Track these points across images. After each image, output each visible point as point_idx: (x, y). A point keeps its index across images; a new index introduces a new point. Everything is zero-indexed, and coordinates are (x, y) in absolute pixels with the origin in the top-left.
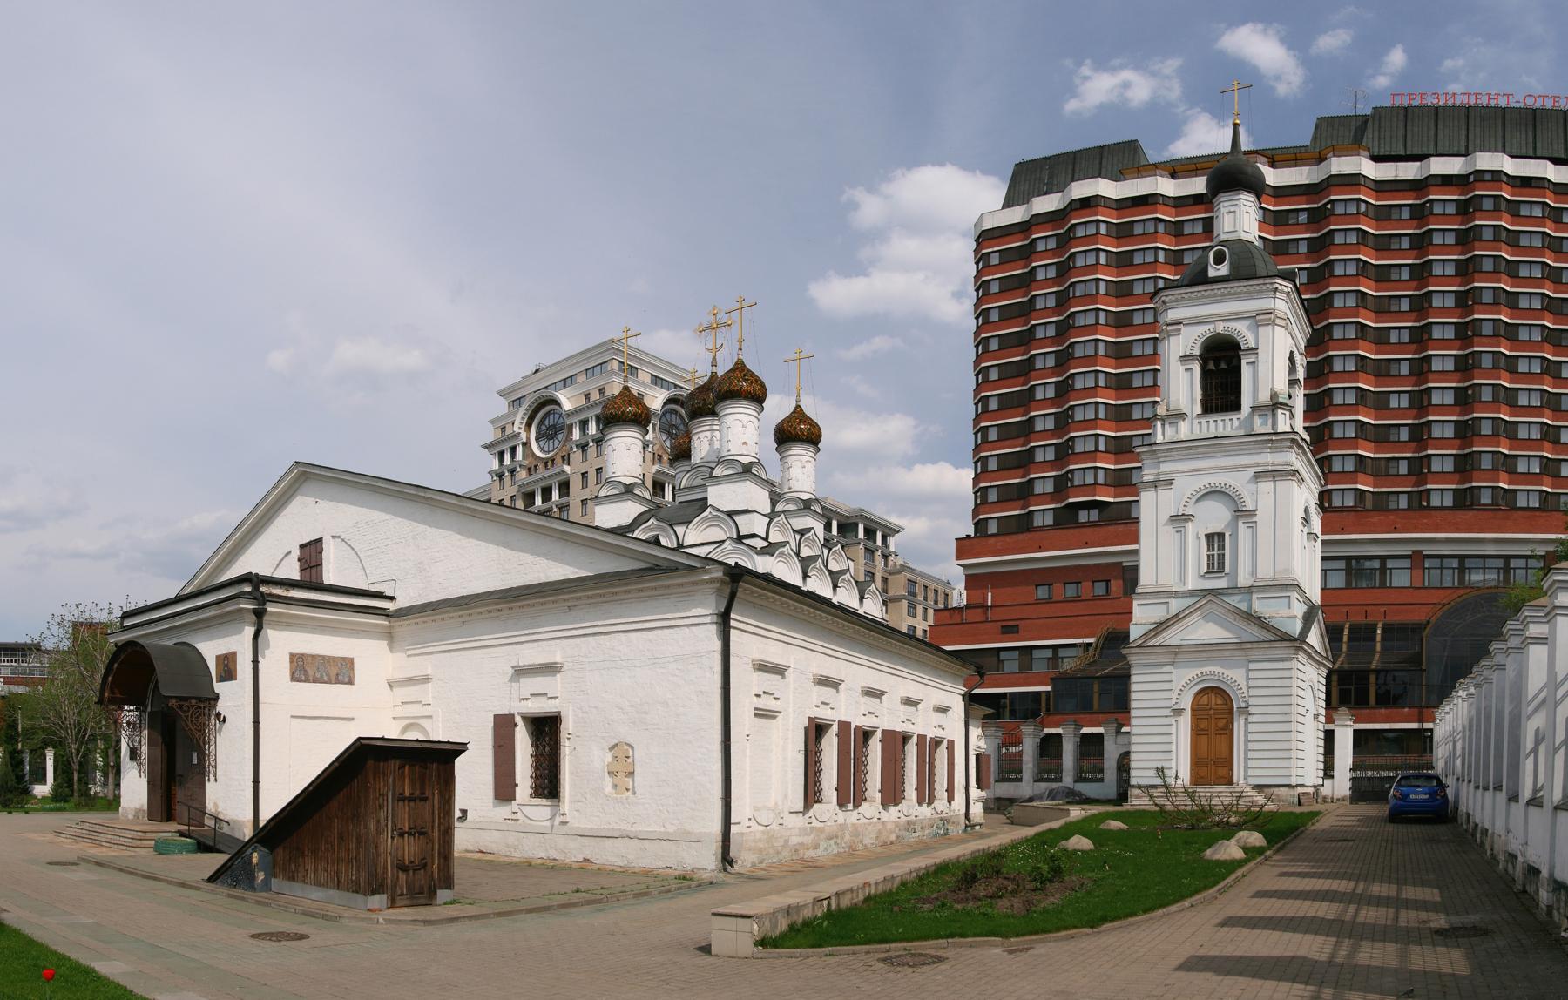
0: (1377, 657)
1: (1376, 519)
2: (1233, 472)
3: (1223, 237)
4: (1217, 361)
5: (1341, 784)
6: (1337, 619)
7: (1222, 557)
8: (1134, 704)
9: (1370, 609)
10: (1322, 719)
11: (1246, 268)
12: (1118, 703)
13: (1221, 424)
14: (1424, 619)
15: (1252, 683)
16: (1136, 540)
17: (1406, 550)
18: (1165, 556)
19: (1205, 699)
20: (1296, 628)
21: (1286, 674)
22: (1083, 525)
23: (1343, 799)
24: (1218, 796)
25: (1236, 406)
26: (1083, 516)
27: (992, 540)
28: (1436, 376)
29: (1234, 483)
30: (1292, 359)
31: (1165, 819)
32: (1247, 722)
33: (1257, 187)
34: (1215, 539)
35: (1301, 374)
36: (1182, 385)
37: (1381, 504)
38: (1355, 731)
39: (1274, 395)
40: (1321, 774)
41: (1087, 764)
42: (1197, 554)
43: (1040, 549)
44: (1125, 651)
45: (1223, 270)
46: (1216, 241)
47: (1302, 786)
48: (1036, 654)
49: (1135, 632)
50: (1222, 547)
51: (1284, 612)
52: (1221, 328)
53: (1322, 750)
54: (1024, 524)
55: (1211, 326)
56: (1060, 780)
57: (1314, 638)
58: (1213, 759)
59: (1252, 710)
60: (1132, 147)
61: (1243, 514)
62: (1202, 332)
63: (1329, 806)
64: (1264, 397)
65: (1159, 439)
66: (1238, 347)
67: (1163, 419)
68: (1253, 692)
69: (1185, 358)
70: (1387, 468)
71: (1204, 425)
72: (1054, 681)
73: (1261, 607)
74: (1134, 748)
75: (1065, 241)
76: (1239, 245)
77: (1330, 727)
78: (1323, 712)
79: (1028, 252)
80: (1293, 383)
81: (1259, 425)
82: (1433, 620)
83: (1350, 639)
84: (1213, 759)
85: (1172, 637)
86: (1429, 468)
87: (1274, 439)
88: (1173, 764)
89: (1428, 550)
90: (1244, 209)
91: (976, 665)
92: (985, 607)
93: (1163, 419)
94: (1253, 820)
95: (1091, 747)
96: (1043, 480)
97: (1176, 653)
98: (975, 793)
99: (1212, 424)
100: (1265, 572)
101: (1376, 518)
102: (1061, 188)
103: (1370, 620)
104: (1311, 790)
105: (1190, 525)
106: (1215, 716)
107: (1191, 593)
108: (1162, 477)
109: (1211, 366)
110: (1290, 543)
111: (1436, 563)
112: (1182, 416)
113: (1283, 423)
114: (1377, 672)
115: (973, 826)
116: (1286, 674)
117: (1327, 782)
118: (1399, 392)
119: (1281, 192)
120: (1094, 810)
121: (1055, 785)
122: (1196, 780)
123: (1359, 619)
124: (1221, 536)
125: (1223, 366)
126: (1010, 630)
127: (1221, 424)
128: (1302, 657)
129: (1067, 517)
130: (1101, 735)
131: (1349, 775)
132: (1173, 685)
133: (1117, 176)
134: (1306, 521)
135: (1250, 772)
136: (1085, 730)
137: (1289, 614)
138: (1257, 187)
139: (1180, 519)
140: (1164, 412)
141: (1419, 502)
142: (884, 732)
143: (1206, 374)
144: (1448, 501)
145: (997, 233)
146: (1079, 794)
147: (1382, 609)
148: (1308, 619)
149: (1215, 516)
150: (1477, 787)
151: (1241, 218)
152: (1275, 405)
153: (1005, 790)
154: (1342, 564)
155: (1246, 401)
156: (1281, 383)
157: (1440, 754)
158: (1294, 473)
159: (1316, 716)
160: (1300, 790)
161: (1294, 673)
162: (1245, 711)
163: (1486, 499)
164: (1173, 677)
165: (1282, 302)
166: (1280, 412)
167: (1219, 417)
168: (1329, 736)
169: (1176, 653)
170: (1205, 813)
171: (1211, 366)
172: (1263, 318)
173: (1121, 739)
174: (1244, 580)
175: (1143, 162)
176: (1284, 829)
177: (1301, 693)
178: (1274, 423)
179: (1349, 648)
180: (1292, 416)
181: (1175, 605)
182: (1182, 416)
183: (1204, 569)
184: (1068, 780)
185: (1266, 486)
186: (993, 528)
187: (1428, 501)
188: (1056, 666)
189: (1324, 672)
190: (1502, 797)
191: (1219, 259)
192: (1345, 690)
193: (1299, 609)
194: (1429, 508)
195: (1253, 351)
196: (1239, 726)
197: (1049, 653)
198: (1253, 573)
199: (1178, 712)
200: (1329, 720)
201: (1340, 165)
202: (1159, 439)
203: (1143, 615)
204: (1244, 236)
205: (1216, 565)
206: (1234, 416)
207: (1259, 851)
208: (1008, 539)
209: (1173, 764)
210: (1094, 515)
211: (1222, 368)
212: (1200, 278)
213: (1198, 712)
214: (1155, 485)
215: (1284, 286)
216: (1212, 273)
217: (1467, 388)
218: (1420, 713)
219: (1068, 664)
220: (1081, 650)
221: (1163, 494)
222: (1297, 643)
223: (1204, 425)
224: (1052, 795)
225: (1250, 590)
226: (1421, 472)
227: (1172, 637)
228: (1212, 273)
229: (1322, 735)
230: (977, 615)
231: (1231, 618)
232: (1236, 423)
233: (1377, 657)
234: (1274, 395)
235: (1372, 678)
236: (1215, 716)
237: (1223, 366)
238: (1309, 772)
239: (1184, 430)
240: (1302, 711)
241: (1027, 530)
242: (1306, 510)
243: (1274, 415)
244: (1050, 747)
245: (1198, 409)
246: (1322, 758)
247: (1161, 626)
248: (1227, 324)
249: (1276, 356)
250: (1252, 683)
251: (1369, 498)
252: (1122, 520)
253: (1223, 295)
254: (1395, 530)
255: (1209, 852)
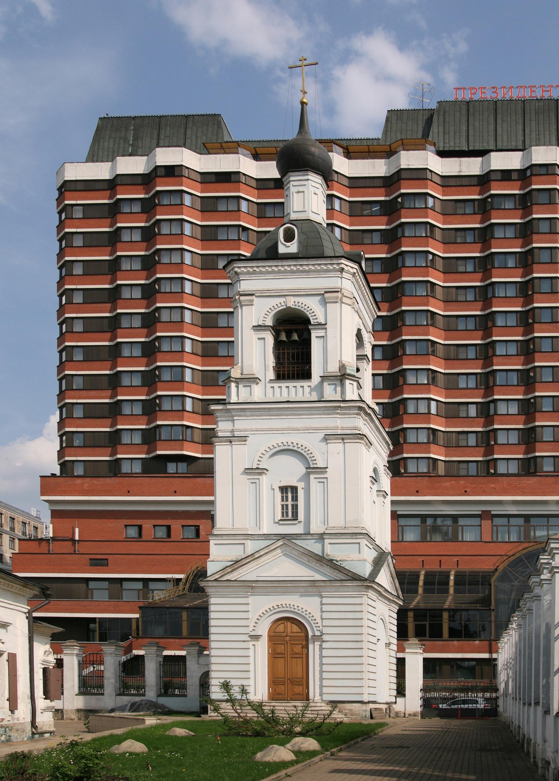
0: (450, 598)
1: (448, 484)
2: (306, 431)
3: (293, 216)
4: (289, 334)
5: (413, 702)
6: (409, 566)
7: (295, 508)
8: (212, 630)
9: (443, 559)
10: (395, 648)
11: (313, 249)
12: (198, 627)
13: (293, 390)
14: (492, 568)
15: (325, 615)
16: (211, 491)
17: (476, 510)
18: (240, 503)
19: (281, 628)
20: (366, 570)
21: (357, 608)
22: (172, 476)
23: (415, 715)
24: (284, 710)
25: (307, 375)
26: (171, 467)
27: (79, 481)
28: (500, 359)
29: (305, 444)
30: (359, 335)
31: (233, 729)
32: (321, 648)
33: (327, 174)
34: (288, 491)
35: (368, 350)
36: (256, 352)
37: (454, 471)
38: (425, 659)
39: (342, 367)
40: (394, 693)
41: (131, 681)
42: (271, 504)
43: (129, 493)
44: (202, 584)
45: (293, 247)
46: (286, 220)
47: (374, 702)
48: (126, 585)
49: (212, 568)
50: (295, 498)
51: (355, 556)
52: (291, 302)
53: (394, 674)
54: (114, 468)
55: (282, 300)
56: (144, 695)
57: (384, 578)
58: (289, 678)
59: (325, 638)
60: (214, 121)
61: (313, 470)
62: (278, 304)
63: (398, 720)
64: (333, 368)
65: (234, 399)
66: (308, 321)
67: (238, 381)
68: (326, 623)
69: (258, 328)
70: (458, 440)
71: (277, 390)
72: (142, 609)
73: (332, 550)
74: (213, 667)
75: (149, 206)
76: (307, 224)
77: (400, 655)
78: (395, 641)
79: (114, 211)
80: (361, 358)
81: (330, 392)
82: (501, 568)
83: (425, 583)
84: (289, 678)
85: (247, 573)
86: (495, 440)
87: (341, 406)
88: (251, 682)
89: (495, 510)
90: (312, 190)
91: (44, 591)
92: (73, 540)
93: (238, 381)
94: (314, 730)
95: (173, 667)
96: (132, 426)
97: (252, 587)
98: (41, 702)
99: (285, 390)
100: (336, 521)
101: (448, 483)
102: (148, 152)
103: (444, 568)
104: (384, 707)
105: (264, 478)
106: (290, 642)
107: (266, 536)
108: (236, 434)
109: (283, 337)
110: (359, 496)
111: (504, 521)
112: (255, 380)
113: (351, 392)
114: (453, 612)
115: (42, 734)
116: (357, 608)
117: (400, 700)
118: (467, 374)
119: (356, 183)
120: (168, 719)
121: (137, 699)
122: (274, 696)
123: (435, 567)
124: (294, 489)
125: (295, 337)
126: (99, 563)
127: (293, 390)
128: (371, 594)
129: (156, 466)
130: (183, 658)
131: (420, 694)
132: (250, 615)
133: (205, 149)
134: (375, 480)
135: (325, 690)
136: (166, 653)
137: (361, 559)
138: (327, 174)
139: (255, 472)
140: (239, 376)
141: (488, 468)
142: (9, 653)
143: (278, 344)
144: (513, 468)
145: (465, 182)
146: (163, 707)
147: (455, 559)
148: (378, 563)
149: (290, 471)
150: (524, 704)
151: (308, 198)
152: (342, 376)
153: (94, 702)
154: (417, 521)
155: (317, 370)
156: (348, 355)
157: (504, 677)
158: (361, 436)
159: (388, 645)
160: (372, 706)
161: (365, 608)
162: (319, 638)
163: (548, 467)
164: (250, 608)
165: (347, 281)
166: (348, 382)
167: (291, 384)
168: (401, 663)
169: (252, 587)
170: (273, 720)
171: (283, 337)
172: (326, 296)
173: (202, 660)
174: (316, 527)
175: (226, 139)
176: (344, 737)
177: (371, 624)
178: (343, 392)
179: (456, 591)
180: (360, 387)
181: (251, 546)
182: (255, 380)
183: (279, 516)
184: (151, 694)
185: (336, 447)
186: (79, 470)
187: (495, 469)
188: (145, 597)
189: (396, 608)
190: (540, 709)
191: (289, 237)
192: (414, 624)
193: (370, 555)
194: (496, 474)
195: (322, 326)
196: (314, 649)
197: (140, 585)
198: (325, 521)
199: (256, 638)
200: (401, 649)
201: (409, 159)
202: (234, 399)
203: (219, 555)
204: (313, 217)
205: (291, 514)
206: (305, 383)
207: (312, 754)
208: (95, 481)
209: (251, 682)
210: (182, 467)
211: (293, 341)
212: (272, 254)
213: (274, 638)
214: (230, 440)
215: (350, 267)
216: (282, 249)
217: (528, 371)
218: (490, 645)
219: (159, 595)
220: (140, 585)
221: (238, 448)
222: (367, 582)
223: (277, 390)
224: (134, 707)
225: (321, 537)
226: (488, 444)
227: (247, 573)
228: (282, 249)
229: (395, 661)
230: (67, 547)
231: (305, 559)
232: (307, 390)
233: (450, 598)
234: (342, 367)
235: (445, 615)
236: (290, 642)
237: (295, 337)
238: (382, 690)
239: (258, 393)
240: (374, 640)
241: (115, 475)
242: (375, 470)
243: (343, 385)
244: (133, 667)
245: (271, 375)
246: (394, 680)
247: (237, 564)
248: (297, 299)
249: (345, 328)
250: (325, 615)
251: (441, 466)
252: (203, 470)
253: (292, 272)
254: (466, 493)
255: (259, 755)
